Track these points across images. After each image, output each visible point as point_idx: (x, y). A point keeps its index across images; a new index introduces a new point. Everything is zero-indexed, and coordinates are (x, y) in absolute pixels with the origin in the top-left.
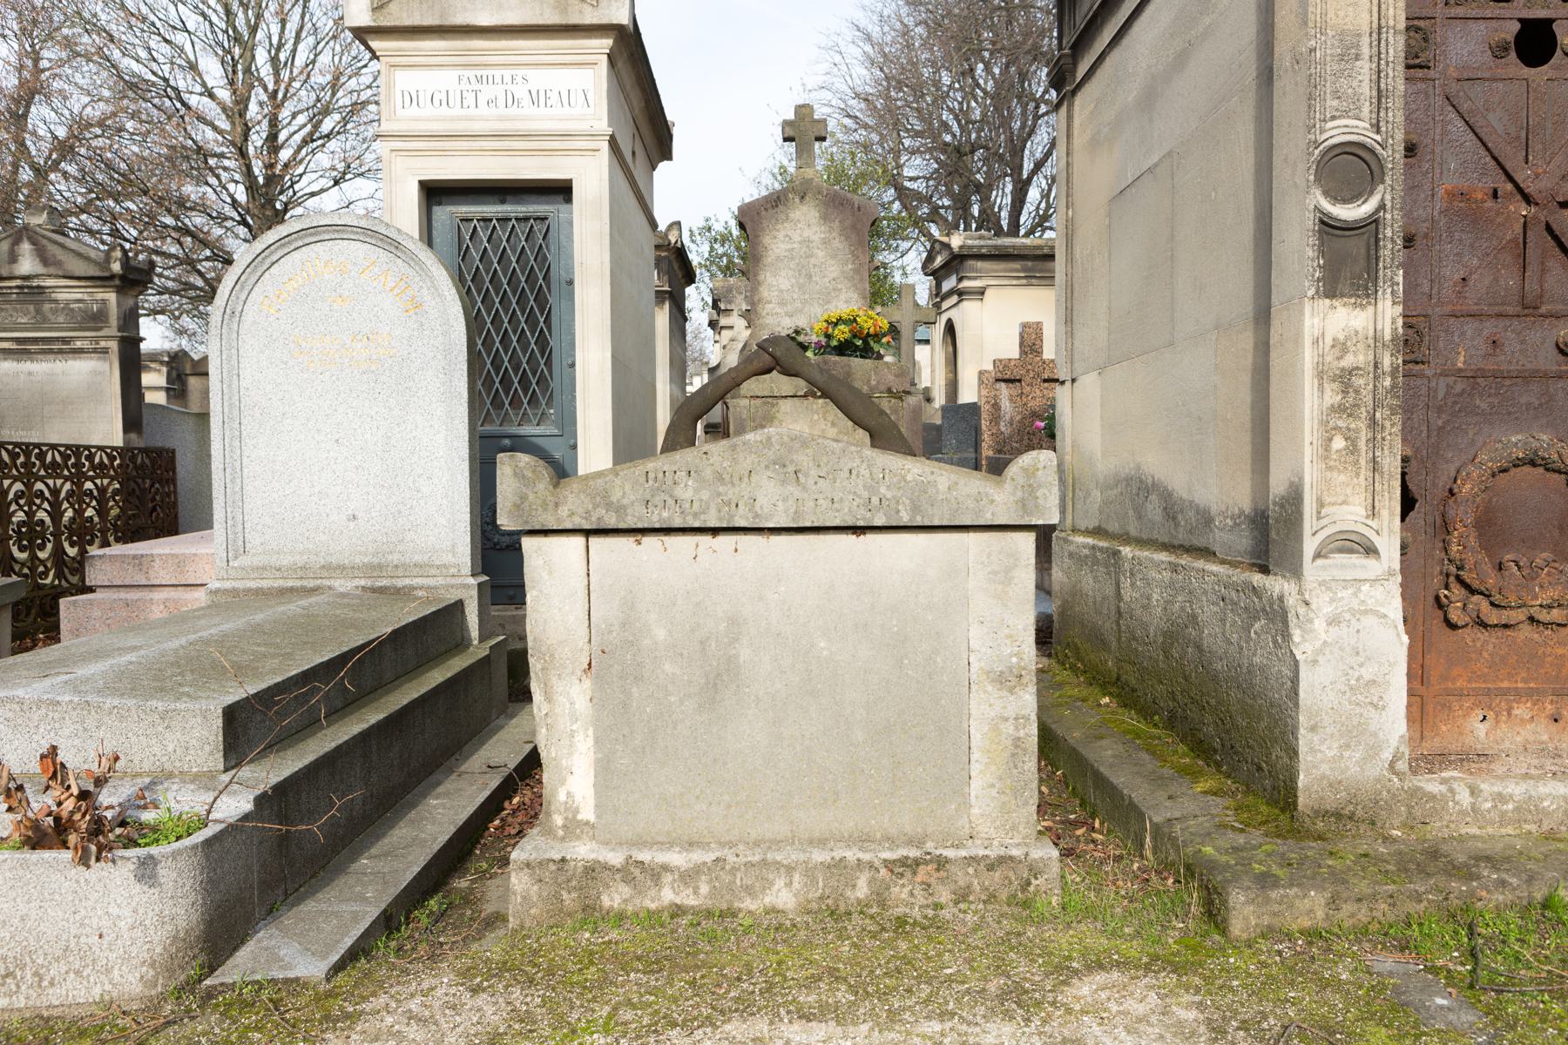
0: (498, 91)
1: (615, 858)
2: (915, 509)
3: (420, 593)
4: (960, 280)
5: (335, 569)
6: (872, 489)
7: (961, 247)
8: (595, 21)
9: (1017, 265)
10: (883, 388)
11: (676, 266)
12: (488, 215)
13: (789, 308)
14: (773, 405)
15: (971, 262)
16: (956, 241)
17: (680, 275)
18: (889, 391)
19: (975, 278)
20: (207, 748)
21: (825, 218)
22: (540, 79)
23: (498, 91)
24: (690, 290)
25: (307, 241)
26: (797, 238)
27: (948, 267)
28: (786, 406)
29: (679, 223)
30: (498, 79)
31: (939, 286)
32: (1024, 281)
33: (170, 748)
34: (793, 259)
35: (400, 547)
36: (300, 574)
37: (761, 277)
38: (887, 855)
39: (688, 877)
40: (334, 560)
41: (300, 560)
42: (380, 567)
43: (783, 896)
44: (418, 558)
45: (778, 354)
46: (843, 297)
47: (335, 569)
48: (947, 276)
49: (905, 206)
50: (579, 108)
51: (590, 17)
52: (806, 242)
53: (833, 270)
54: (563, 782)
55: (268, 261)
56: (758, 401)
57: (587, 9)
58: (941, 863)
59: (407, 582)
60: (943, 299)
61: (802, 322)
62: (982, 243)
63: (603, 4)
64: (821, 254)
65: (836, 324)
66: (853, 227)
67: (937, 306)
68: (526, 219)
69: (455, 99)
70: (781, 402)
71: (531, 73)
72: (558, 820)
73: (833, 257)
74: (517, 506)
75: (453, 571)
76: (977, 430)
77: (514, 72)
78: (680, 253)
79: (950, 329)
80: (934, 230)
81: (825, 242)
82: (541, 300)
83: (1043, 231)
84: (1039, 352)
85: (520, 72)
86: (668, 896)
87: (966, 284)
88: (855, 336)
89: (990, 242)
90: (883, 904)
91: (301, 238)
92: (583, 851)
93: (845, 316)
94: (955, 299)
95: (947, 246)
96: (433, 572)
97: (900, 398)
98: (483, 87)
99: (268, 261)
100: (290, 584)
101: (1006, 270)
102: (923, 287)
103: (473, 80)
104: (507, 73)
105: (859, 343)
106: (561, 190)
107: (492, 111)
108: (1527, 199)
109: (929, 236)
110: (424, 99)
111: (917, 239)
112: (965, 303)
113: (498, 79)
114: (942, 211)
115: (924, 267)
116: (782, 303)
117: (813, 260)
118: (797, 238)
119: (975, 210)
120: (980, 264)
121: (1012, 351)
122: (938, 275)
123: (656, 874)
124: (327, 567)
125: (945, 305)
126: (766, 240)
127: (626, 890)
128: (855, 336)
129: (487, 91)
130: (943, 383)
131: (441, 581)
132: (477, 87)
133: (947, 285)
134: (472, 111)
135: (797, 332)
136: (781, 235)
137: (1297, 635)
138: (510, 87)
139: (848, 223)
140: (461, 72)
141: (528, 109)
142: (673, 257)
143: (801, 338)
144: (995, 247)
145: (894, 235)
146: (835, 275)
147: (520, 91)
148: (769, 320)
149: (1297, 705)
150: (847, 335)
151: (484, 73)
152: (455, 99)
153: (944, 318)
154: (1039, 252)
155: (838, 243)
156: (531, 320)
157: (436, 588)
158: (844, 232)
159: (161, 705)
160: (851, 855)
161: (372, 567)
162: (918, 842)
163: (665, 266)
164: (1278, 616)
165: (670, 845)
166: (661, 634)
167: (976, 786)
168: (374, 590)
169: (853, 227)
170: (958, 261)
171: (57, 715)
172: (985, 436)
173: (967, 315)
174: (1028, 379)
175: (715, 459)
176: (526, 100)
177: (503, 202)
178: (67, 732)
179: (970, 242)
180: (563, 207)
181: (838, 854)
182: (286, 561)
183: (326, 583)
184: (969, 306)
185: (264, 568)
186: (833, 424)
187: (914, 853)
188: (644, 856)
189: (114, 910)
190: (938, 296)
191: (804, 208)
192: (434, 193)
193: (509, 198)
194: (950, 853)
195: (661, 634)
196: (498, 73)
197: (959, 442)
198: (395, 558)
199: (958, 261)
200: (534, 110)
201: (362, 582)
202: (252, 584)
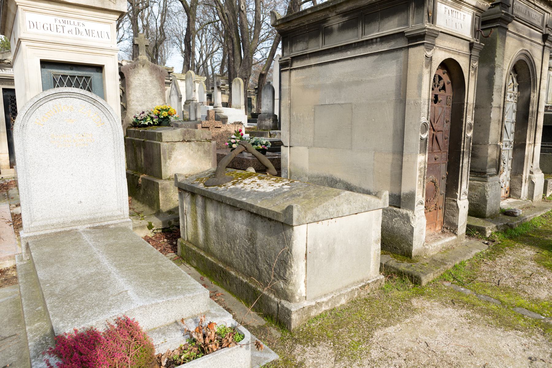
0: (73, 28)
1: (313, 303)
2: (368, 207)
3: (111, 227)
5: (77, 222)
6: (362, 204)
8: (115, 9)
10: (204, 138)
20: (205, 304)
21: (151, 73)
22: (90, 26)
23: (73, 28)
25: (55, 97)
26: (142, 80)
28: (178, 144)
30: (72, 23)
33: (194, 308)
34: (141, 86)
35: (100, 211)
36: (62, 226)
38: (360, 286)
39: (327, 303)
40: (75, 218)
41: (61, 221)
42: (94, 219)
43: (343, 301)
46: (158, 100)
47: (77, 222)
50: (105, 39)
51: (112, 7)
52: (145, 81)
54: (299, 288)
55: (39, 105)
56: (169, 143)
57: (112, 4)
58: (368, 284)
59: (106, 223)
63: (118, 2)
64: (150, 85)
66: (160, 77)
68: (82, 77)
69: (54, 28)
70: (176, 143)
71: (86, 23)
72: (297, 298)
73: (154, 87)
74: (298, 219)
75: (122, 217)
77: (79, 21)
81: (151, 82)
85: (81, 22)
86: (323, 309)
90: (360, 297)
91: (53, 96)
92: (306, 304)
96: (115, 218)
98: (66, 25)
99: (39, 105)
100: (59, 230)
103: (61, 22)
104: (76, 22)
106: (99, 68)
107: (70, 35)
108: (434, 130)
110: (40, 26)
113: (72, 23)
116: (138, 101)
117: (147, 87)
118: (142, 80)
123: (319, 304)
124: (73, 222)
126: (131, 79)
127: (315, 310)
129: (68, 27)
132: (64, 25)
134: (61, 34)
136: (136, 78)
137: (412, 222)
138: (77, 27)
139: (158, 76)
140: (56, 18)
141: (85, 36)
146: (154, 93)
147: (82, 29)
149: (413, 236)
151: (66, 20)
152: (54, 28)
157: (117, 224)
158: (157, 78)
159: (191, 295)
160: (354, 288)
161: (92, 220)
162: (362, 281)
164: (407, 219)
165: (321, 297)
166: (321, 245)
167: (371, 266)
168: (94, 228)
171: (158, 308)
175: (336, 201)
176: (84, 33)
177: (72, 69)
178: (161, 312)
181: (352, 288)
182: (55, 221)
183: (74, 228)
185: (46, 226)
186: (192, 150)
187: (364, 284)
188: (319, 301)
189: (241, 361)
191: (144, 70)
192: (45, 64)
194: (369, 282)
195: (321, 245)
196: (72, 21)
198: (99, 215)
200: (87, 37)
201: (89, 226)
202: (43, 233)
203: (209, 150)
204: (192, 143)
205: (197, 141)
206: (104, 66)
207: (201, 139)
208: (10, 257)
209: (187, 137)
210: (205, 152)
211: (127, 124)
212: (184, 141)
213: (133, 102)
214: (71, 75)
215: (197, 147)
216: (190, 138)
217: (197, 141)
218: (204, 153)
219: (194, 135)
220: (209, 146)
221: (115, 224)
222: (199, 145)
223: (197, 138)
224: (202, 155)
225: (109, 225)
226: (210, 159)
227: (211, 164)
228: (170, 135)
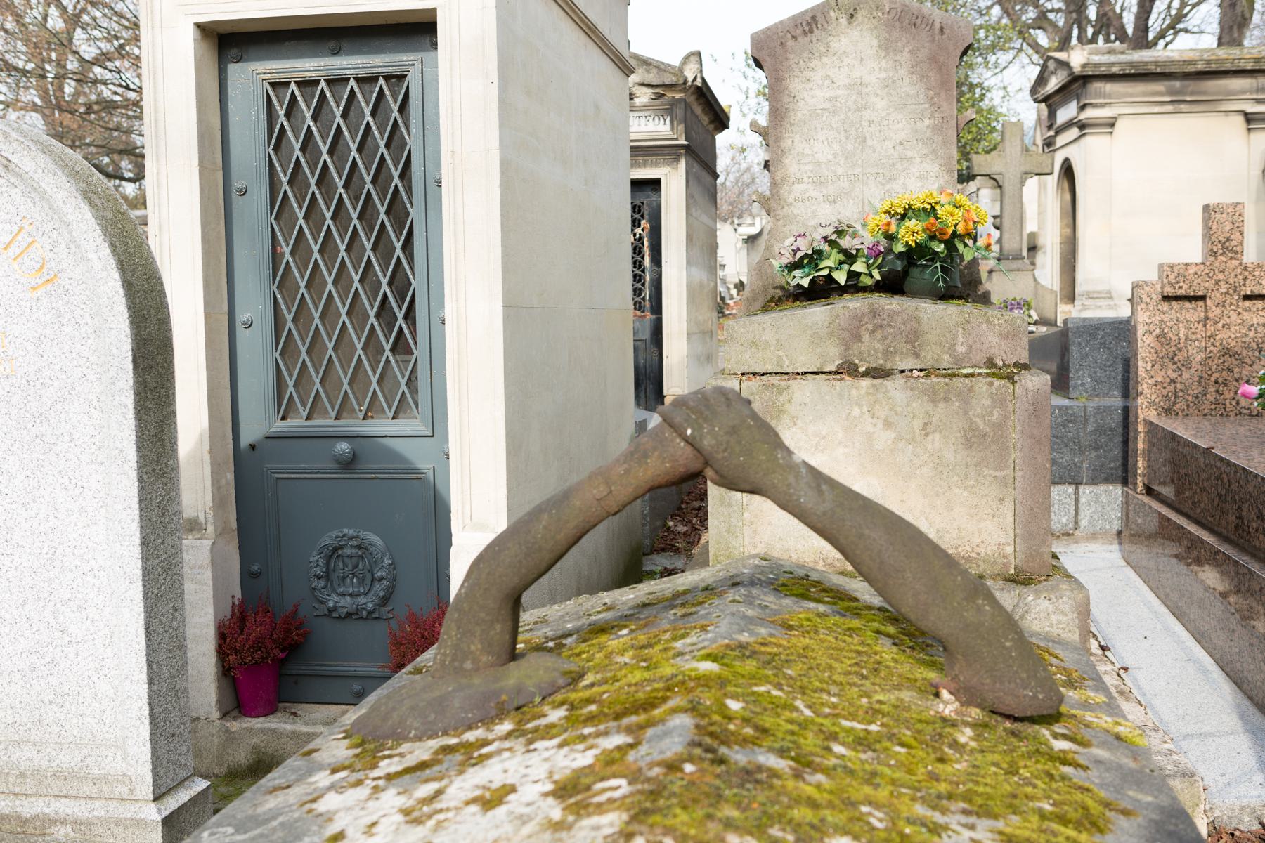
4: (1083, 108)
7: (1084, 66)
9: (1160, 86)
10: (980, 358)
11: (698, 110)
12: (313, 75)
13: (831, 190)
14: (780, 391)
15: (1098, 86)
16: (1078, 58)
17: (705, 119)
18: (990, 363)
19: (1103, 105)
21: (887, 47)
24: (722, 139)
27: (1065, 91)
28: (803, 390)
29: (699, 54)
31: (1052, 115)
32: (1169, 108)
34: (835, 112)
37: (787, 143)
44: (64, 760)
45: (707, 443)
48: (1064, 102)
49: (1006, 11)
53: (900, 128)
59: (39, 807)
60: (1057, 133)
61: (848, 213)
62: (1113, 58)
64: (880, 104)
65: (903, 217)
66: (933, 60)
67: (1049, 143)
68: (372, 79)
70: (796, 384)
75: (121, 790)
76: (1128, 366)
78: (703, 94)
79: (1068, 171)
80: (1043, 39)
81: (887, 85)
82: (397, 211)
83: (1176, 34)
84: (1236, 253)
87: (1084, 116)
88: (932, 238)
89: (1123, 58)
93: (917, 205)
94: (1074, 132)
95: (1065, 65)
96: (86, 789)
97: (1010, 378)
101: (1145, 94)
102: (1027, 112)
105: (940, 248)
106: (418, 30)
109: (1036, 46)
111: (1020, 50)
112: (1088, 139)
114: (1051, 16)
115: (1033, 91)
116: (819, 182)
117: (867, 114)
119: (1092, 12)
120: (1109, 87)
121: (1191, 250)
122: (1051, 102)
125: (1061, 140)
128: (932, 238)
130: (1057, 240)
131: (98, 809)
133: (1064, 115)
135: (840, 233)
136: (817, 76)
139: (924, 53)
142: (691, 99)
143: (845, 242)
144: (1131, 64)
145: (993, 48)
146: (902, 136)
148: (799, 209)
150: (921, 237)
153: (1059, 158)
154: (1191, 69)
155: (909, 87)
156: (381, 242)
163: (679, 112)
169: (933, 60)
170: (1078, 84)
172: (1144, 387)
173: (1088, 154)
174: (1216, 296)
177: (336, 52)
179: (1096, 59)
180: (426, 56)
184: (1095, 141)
186: (888, 424)
190: (1051, 125)
191: (855, 33)
193: (345, 44)
197: (1097, 381)
199: (1078, 84)
203: (1000, 427)
204: (894, 386)
205: (927, 372)
206: (433, 12)
207: (958, 360)
208: (937, 780)
209: (869, 351)
210: (973, 439)
211: (765, 288)
212: (847, 370)
213: (798, 189)
214: (332, 74)
215: (920, 406)
216: (887, 353)
217: (927, 372)
218: (969, 445)
219: (914, 338)
220: (998, 401)
221: (76, 823)
222: (933, 397)
223: (933, 354)
224: (949, 455)
225: (49, 821)
226: (1003, 482)
227: (1008, 509)
228: (768, 336)
